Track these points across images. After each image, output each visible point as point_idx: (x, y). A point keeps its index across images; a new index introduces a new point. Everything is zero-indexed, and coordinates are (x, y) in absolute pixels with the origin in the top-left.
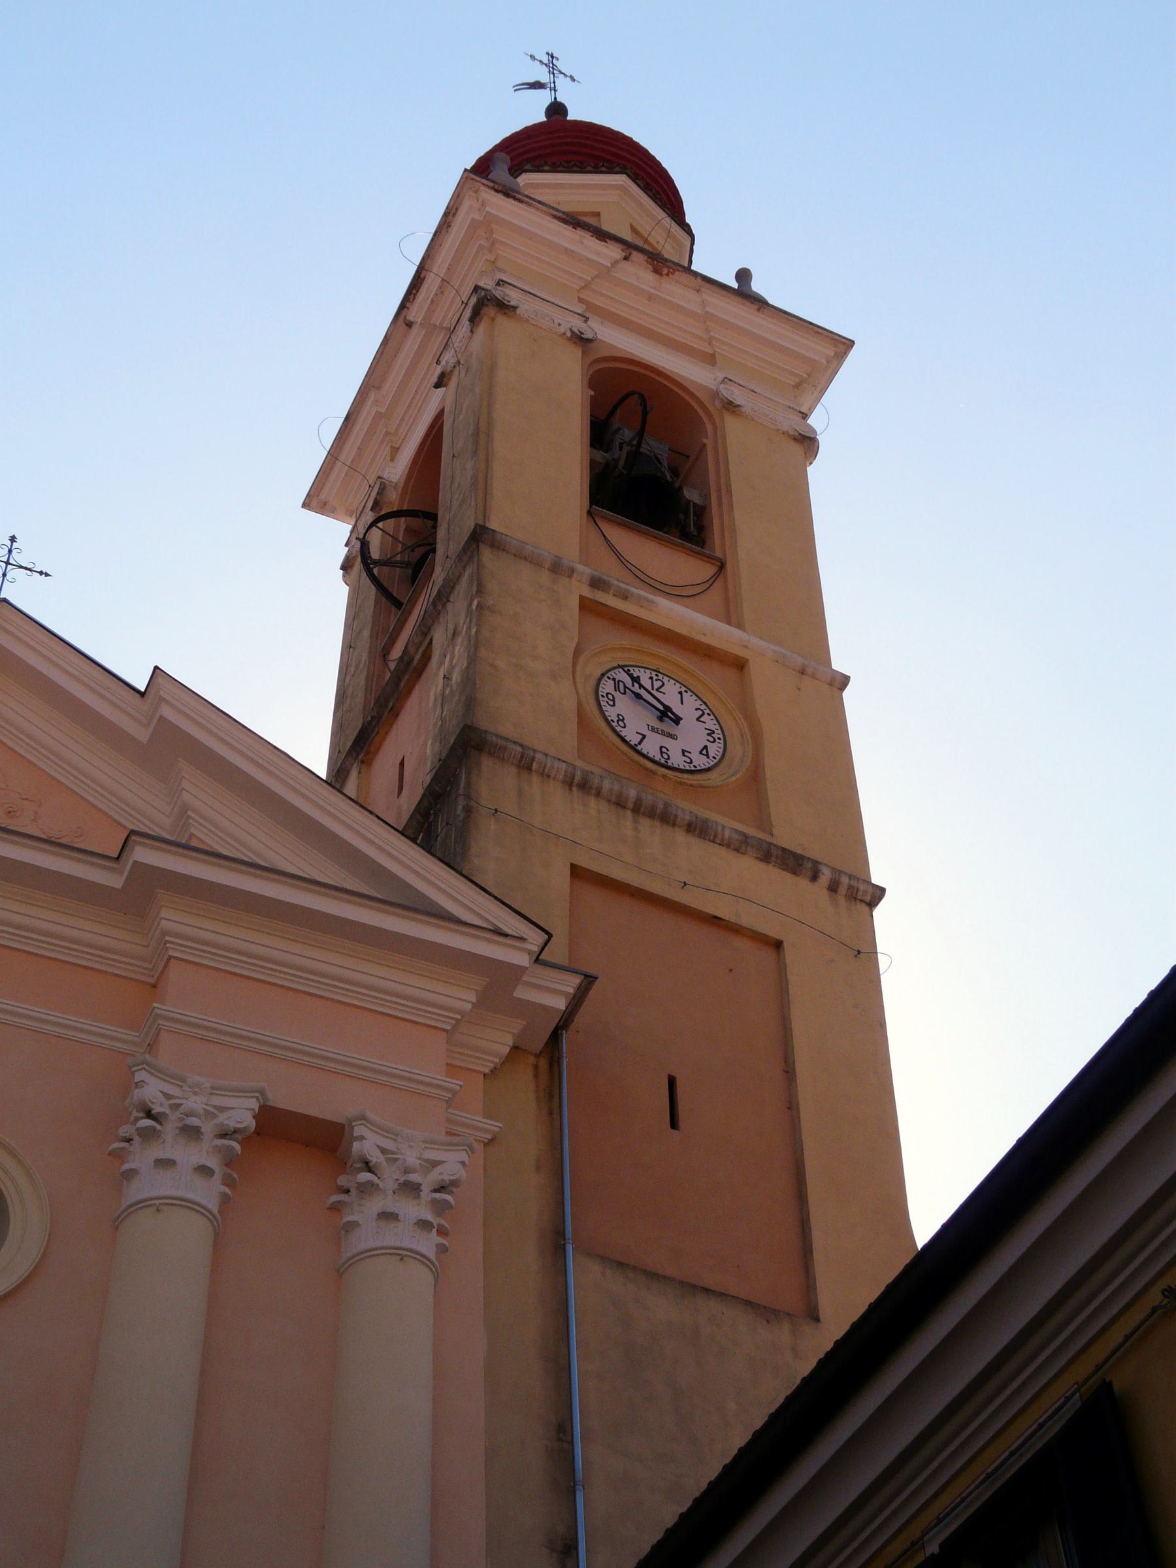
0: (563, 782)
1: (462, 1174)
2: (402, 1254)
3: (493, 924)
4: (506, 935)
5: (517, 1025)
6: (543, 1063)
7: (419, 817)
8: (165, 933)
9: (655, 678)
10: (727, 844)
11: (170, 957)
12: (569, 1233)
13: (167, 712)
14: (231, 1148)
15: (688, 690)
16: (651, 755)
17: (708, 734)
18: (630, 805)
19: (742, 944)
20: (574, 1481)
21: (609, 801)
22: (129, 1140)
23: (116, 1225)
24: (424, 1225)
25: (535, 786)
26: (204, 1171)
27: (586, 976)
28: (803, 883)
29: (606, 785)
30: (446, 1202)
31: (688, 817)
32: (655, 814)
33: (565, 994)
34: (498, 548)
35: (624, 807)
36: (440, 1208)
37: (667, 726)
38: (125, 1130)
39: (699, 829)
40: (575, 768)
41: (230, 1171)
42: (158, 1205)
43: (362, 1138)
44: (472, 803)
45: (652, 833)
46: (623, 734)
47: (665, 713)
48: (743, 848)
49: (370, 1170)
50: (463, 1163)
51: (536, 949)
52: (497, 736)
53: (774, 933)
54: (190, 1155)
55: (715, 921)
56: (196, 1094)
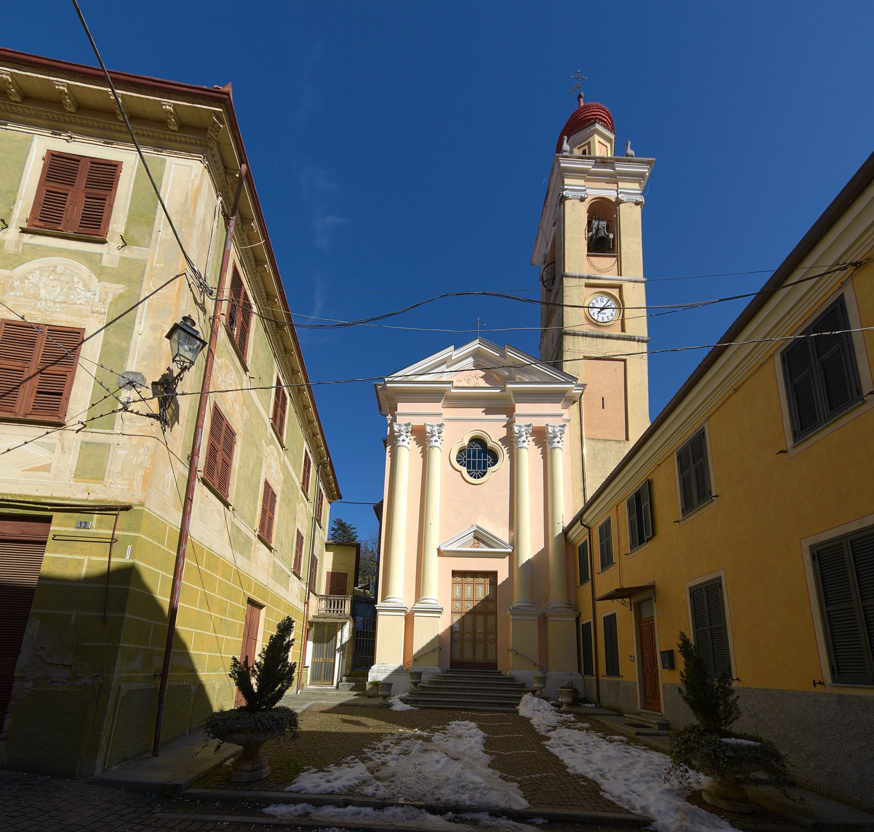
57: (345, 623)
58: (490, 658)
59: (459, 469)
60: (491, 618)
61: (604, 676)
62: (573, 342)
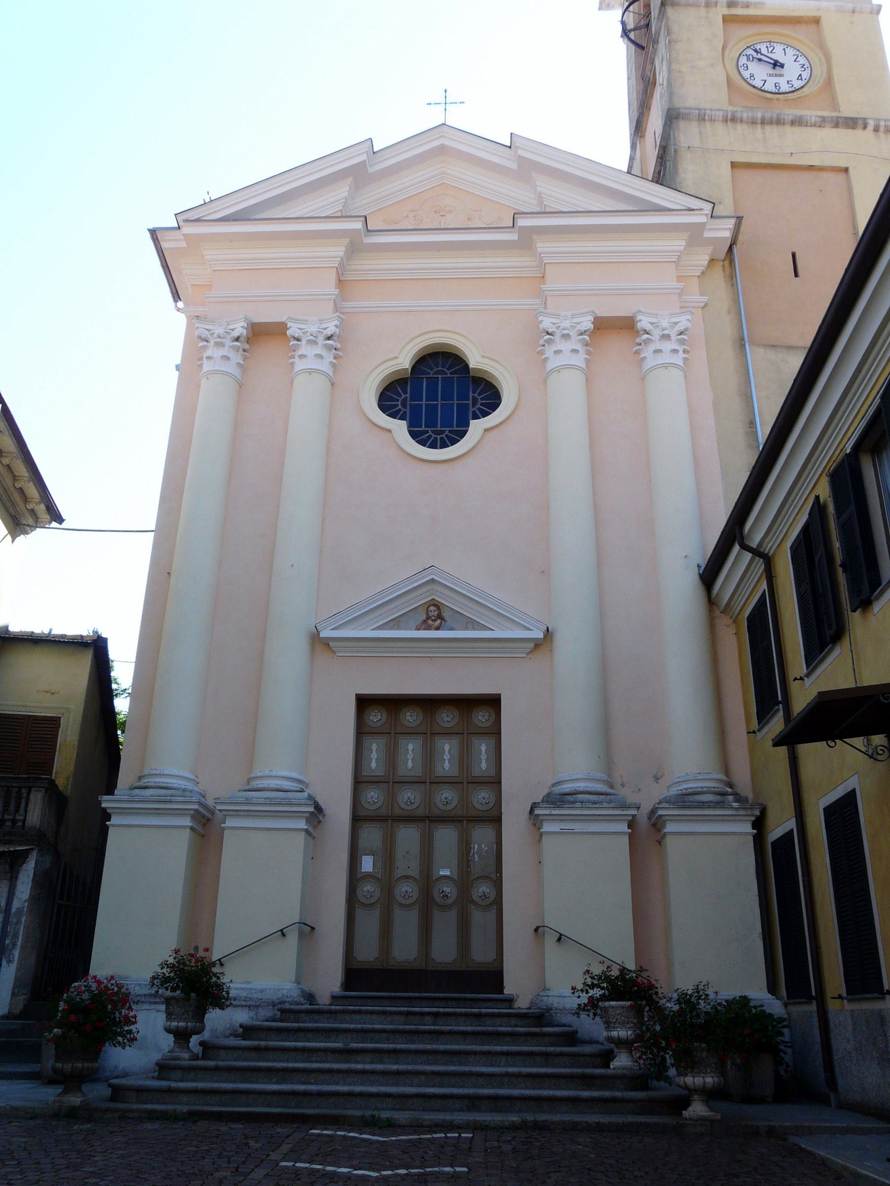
0: (723, 121)
1: (689, 325)
2: (666, 366)
3: (687, 207)
4: (693, 210)
5: (710, 249)
6: (727, 263)
7: (660, 160)
8: (540, 254)
9: (769, 46)
10: (814, 125)
11: (545, 263)
12: (746, 339)
13: (521, 153)
14: (584, 339)
15: (788, 46)
16: (770, 90)
17: (802, 67)
18: (759, 121)
19: (826, 175)
20: (758, 443)
21: (747, 123)
22: (544, 345)
23: (545, 380)
24: (675, 351)
25: (708, 127)
26: (575, 351)
27: (737, 218)
28: (859, 133)
29: (745, 115)
30: (684, 339)
31: (790, 118)
32: (773, 122)
33: (729, 229)
34: (676, 5)
35: (756, 123)
36: (682, 342)
37: (778, 70)
38: (541, 342)
39: (797, 122)
40: (727, 111)
41: (588, 348)
42: (558, 370)
43: (640, 320)
44: (677, 147)
45: (772, 131)
46: (753, 84)
47: (776, 64)
48: (823, 125)
49: (648, 334)
50: (688, 320)
51: (709, 212)
52: (685, 108)
53: (843, 164)
54: (566, 346)
55: (811, 168)
56: (565, 320)
57: (25, 855)
58: (481, 954)
59: (388, 426)
60: (481, 836)
61: (840, 997)
62: (700, 133)
